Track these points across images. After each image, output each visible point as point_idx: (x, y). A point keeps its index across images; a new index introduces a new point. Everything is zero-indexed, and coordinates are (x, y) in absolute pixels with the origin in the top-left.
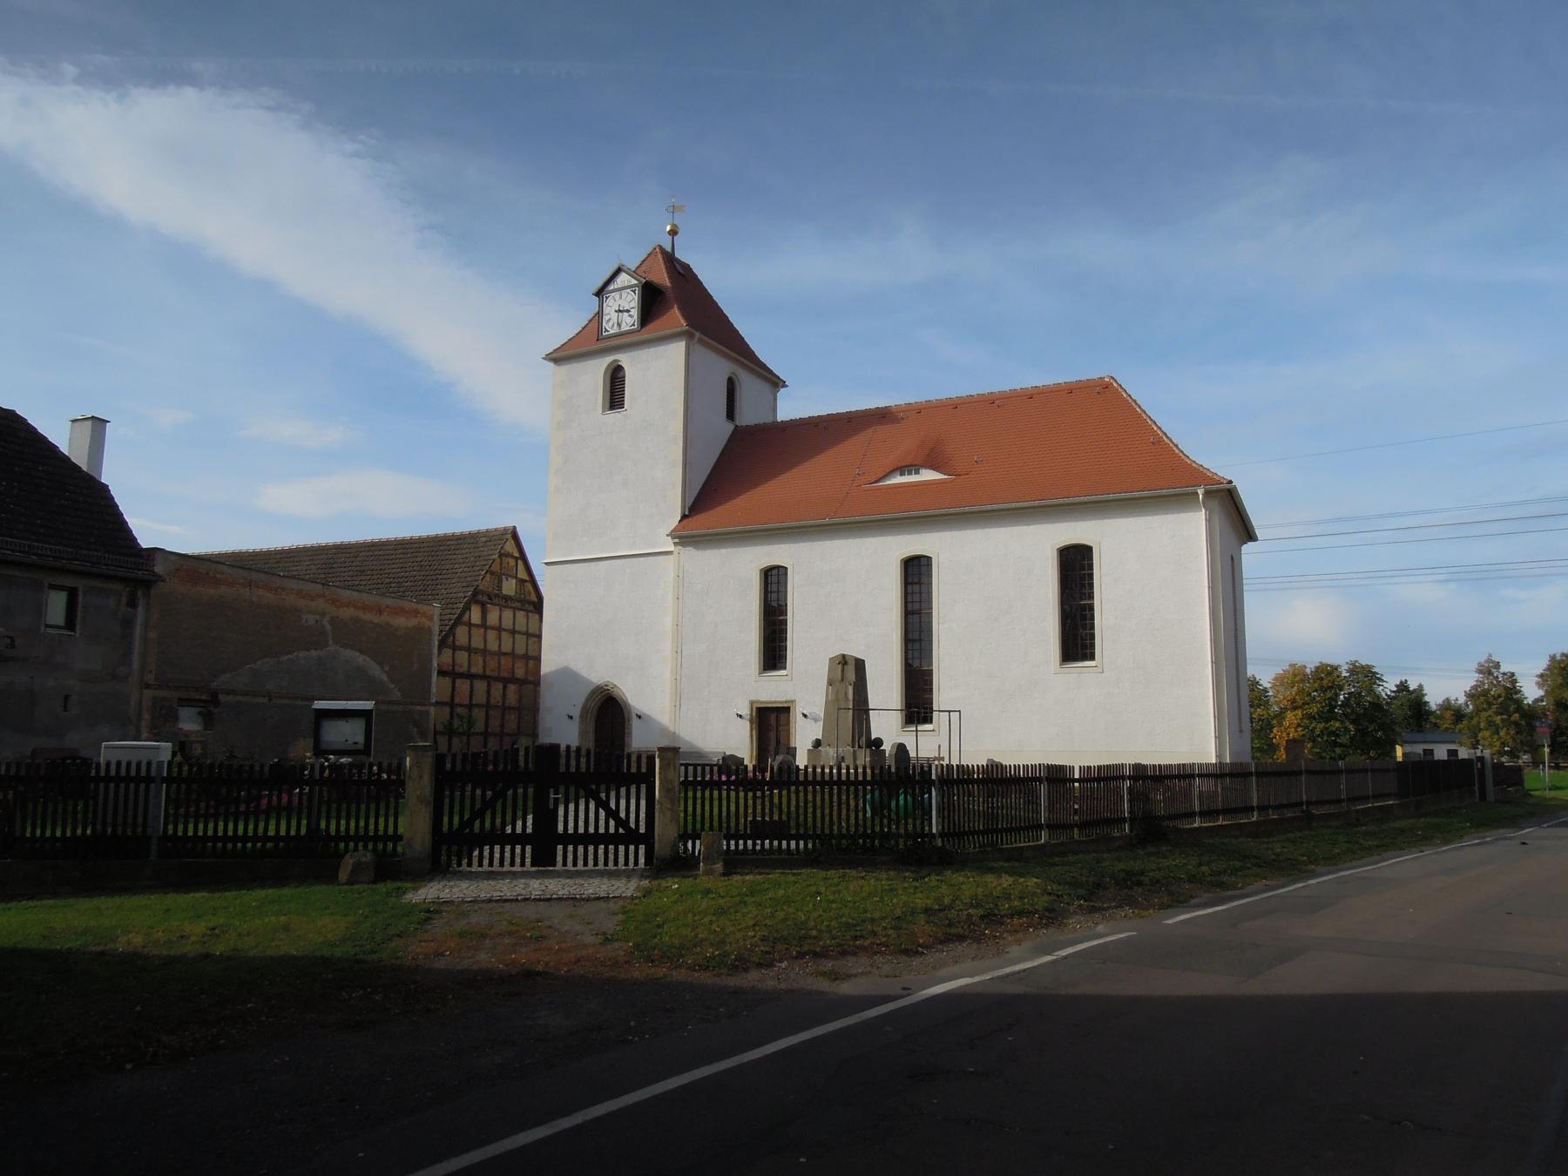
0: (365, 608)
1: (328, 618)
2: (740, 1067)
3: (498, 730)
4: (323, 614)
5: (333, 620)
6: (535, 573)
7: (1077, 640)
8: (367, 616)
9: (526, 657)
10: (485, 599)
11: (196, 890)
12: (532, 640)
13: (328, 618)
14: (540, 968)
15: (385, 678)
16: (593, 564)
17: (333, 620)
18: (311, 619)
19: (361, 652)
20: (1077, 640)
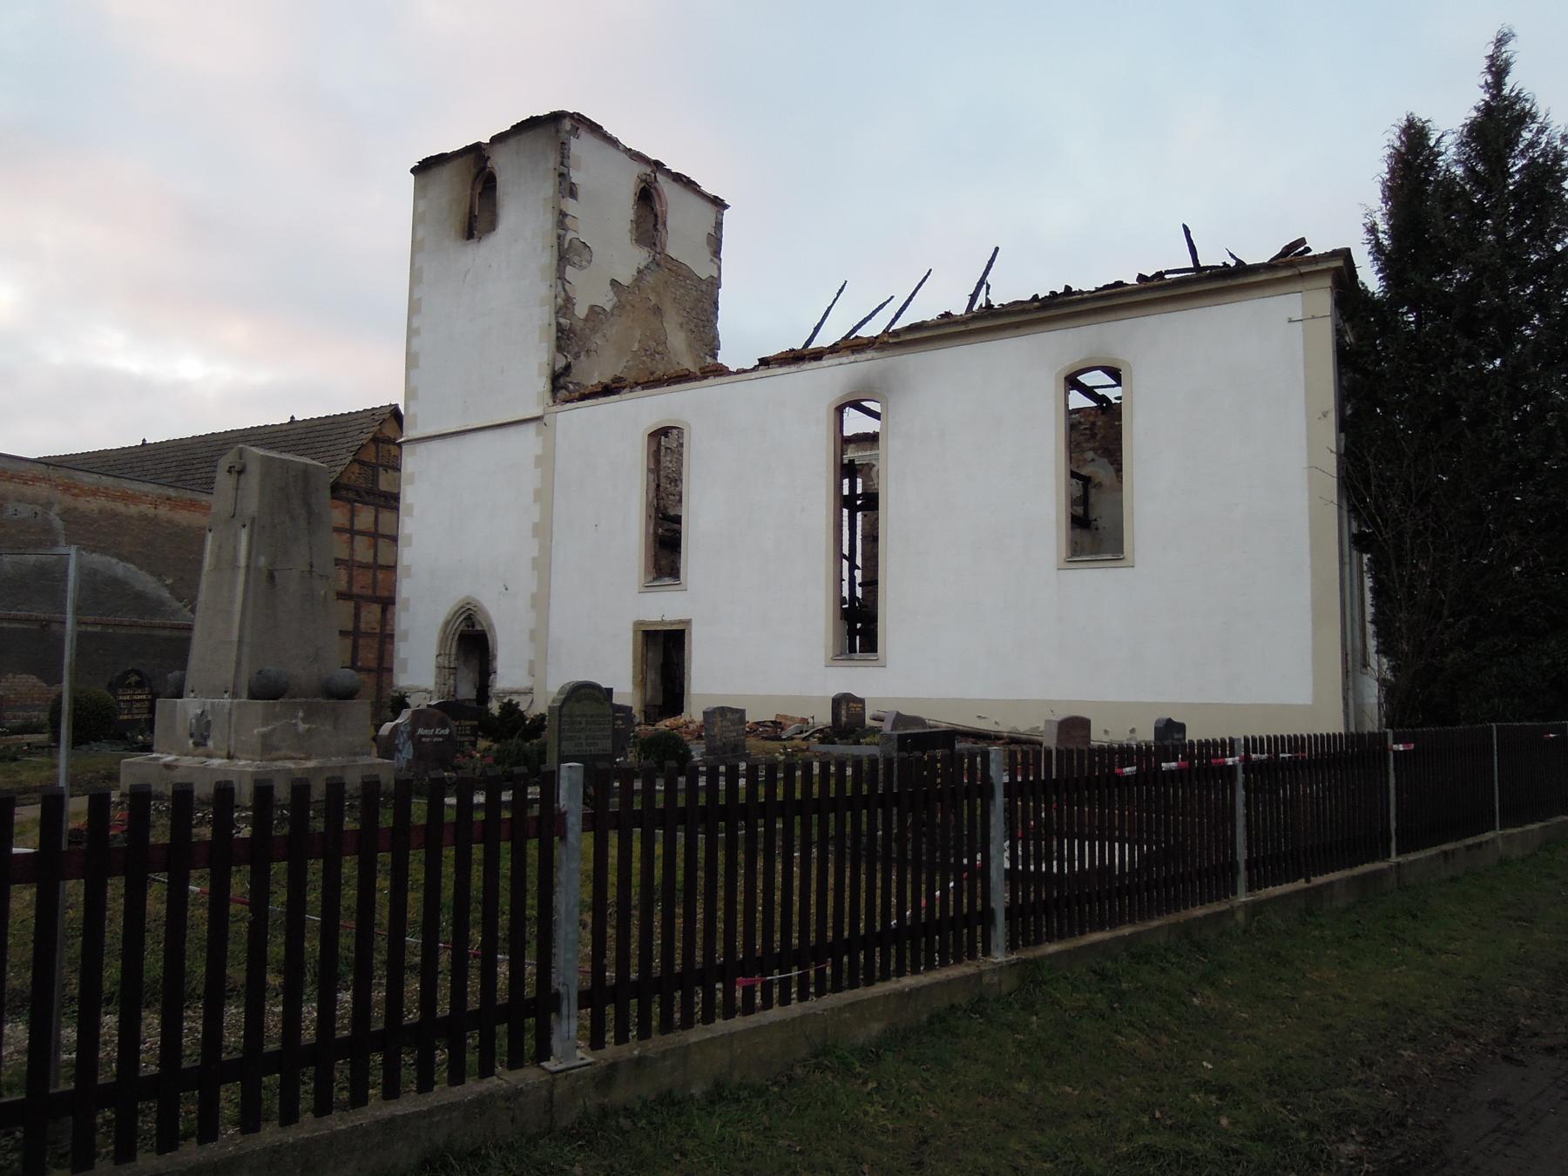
0: (127, 498)
1: (56, 508)
2: (1351, 866)
3: (374, 665)
4: (49, 505)
5: (66, 514)
6: (1341, 716)
7: (1093, 526)
8: (120, 507)
9: (375, 566)
10: (351, 495)
11: (85, 895)
12: (381, 543)
13: (56, 508)
14: (588, 968)
15: (166, 594)
16: (454, 440)
17: (66, 514)
18: (25, 510)
19: (121, 558)
20: (1093, 526)
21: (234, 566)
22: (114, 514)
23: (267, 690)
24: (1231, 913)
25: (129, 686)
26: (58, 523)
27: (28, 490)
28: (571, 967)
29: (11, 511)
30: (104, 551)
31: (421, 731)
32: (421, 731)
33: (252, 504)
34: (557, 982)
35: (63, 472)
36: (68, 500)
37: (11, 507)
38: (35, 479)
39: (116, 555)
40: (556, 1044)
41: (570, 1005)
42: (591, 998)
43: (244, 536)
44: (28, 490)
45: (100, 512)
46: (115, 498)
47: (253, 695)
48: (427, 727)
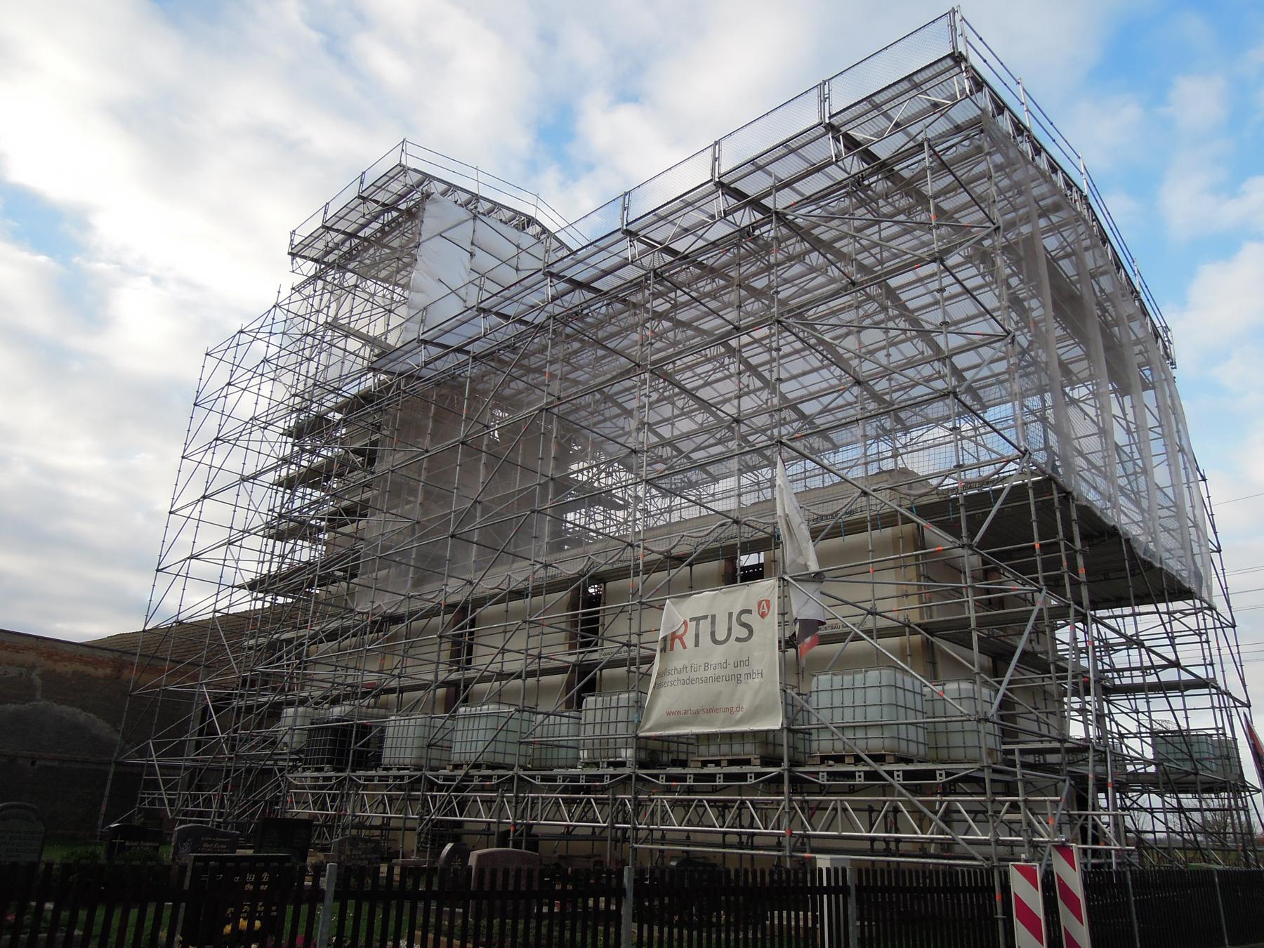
4: (33, 667)
7: (697, 644)
8: (90, 670)
13: (38, 671)
19: (85, 709)
26: (38, 681)
45: (74, 673)
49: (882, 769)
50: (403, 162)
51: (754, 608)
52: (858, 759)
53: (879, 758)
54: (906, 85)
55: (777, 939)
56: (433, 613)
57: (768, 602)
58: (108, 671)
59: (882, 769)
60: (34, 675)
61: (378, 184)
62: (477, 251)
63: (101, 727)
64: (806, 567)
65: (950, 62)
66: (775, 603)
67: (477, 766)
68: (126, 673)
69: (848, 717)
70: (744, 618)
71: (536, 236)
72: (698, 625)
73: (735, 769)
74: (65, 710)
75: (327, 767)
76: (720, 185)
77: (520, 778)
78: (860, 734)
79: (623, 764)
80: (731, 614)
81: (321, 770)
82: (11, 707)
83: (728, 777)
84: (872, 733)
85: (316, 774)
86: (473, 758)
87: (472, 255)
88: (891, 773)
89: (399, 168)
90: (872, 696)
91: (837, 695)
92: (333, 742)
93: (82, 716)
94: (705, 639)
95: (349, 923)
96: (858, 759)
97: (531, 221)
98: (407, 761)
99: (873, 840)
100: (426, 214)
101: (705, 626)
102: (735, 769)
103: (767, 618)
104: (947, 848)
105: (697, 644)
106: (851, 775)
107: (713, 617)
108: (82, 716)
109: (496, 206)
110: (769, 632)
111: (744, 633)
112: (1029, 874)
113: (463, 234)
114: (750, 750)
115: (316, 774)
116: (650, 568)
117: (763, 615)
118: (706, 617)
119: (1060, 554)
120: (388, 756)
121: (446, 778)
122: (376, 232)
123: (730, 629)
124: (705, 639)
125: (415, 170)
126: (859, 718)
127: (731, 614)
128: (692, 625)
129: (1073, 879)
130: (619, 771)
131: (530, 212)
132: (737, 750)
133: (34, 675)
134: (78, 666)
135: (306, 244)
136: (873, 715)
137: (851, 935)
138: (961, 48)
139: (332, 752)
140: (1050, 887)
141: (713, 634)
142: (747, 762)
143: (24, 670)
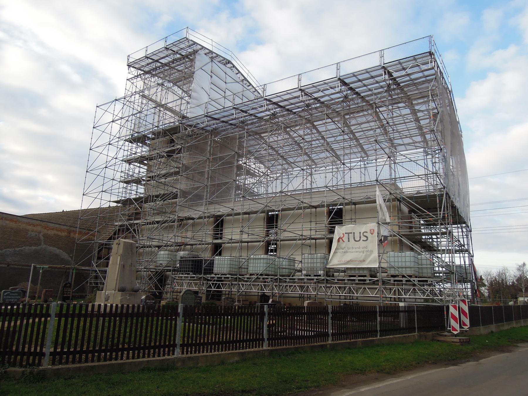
1: (42, 234)
4: (40, 232)
7: (349, 241)
8: (59, 233)
13: (42, 234)
17: (44, 236)
18: (33, 234)
19: (59, 248)
21: (117, 264)
22: (58, 236)
23: (122, 290)
24: (326, 345)
25: (67, 287)
26: (42, 238)
27: (35, 229)
28: (179, 341)
29: (30, 234)
30: (54, 246)
31: (147, 301)
32: (147, 301)
33: (121, 251)
34: (176, 342)
35: (45, 223)
36: (46, 231)
37: (30, 233)
38: (37, 225)
39: (57, 247)
40: (176, 353)
41: (178, 346)
42: (182, 346)
43: (119, 258)
44: (35, 229)
45: (54, 235)
46: (58, 231)
47: (119, 291)
48: (149, 300)
49: (411, 279)
50: (187, 37)
51: (369, 231)
52: (403, 276)
53: (410, 276)
54: (412, 58)
55: (28, 340)
56: (209, 217)
57: (374, 230)
58: (66, 234)
59: (411, 279)
60: (41, 235)
61: (174, 44)
62: (210, 73)
63: (64, 255)
64: (385, 220)
65: (428, 54)
66: (376, 231)
67: (261, 275)
68: (72, 235)
69: (400, 265)
70: (365, 234)
71: (230, 68)
72: (349, 235)
73: (362, 278)
74: (51, 249)
75: (191, 273)
76: (339, 79)
77: (280, 279)
78: (404, 270)
79: (320, 276)
80: (360, 233)
81: (189, 274)
82: (34, 248)
83: (359, 280)
84: (407, 269)
85: (186, 275)
86: (261, 272)
87: (211, 77)
88: (414, 280)
89: (185, 39)
90: (408, 259)
91: (396, 258)
92: (192, 265)
93: (58, 251)
94: (352, 239)
95: (62, 328)
96: (403, 276)
97: (229, 62)
98: (225, 272)
99: (391, 298)
100: (196, 60)
101: (351, 236)
102: (362, 278)
103: (374, 235)
104: (433, 301)
105: (349, 241)
106: (402, 281)
107: (354, 233)
108: (58, 251)
109: (218, 55)
110: (374, 240)
111: (365, 239)
112: (455, 307)
113: (208, 68)
114: (366, 273)
115: (186, 275)
116: (305, 208)
117: (372, 234)
118: (351, 233)
119: (435, 211)
120: (215, 270)
121: (248, 278)
122: (173, 64)
123: (360, 237)
124: (352, 239)
125: (191, 40)
126: (404, 265)
127: (360, 233)
128: (346, 235)
129: (466, 309)
130: (319, 278)
131: (229, 58)
132: (361, 273)
133: (41, 235)
134: (55, 232)
135: (135, 62)
136: (408, 264)
137: (178, 333)
138: (433, 51)
139: (192, 268)
140: (461, 311)
141: (354, 238)
142: (365, 276)
143: (37, 234)
